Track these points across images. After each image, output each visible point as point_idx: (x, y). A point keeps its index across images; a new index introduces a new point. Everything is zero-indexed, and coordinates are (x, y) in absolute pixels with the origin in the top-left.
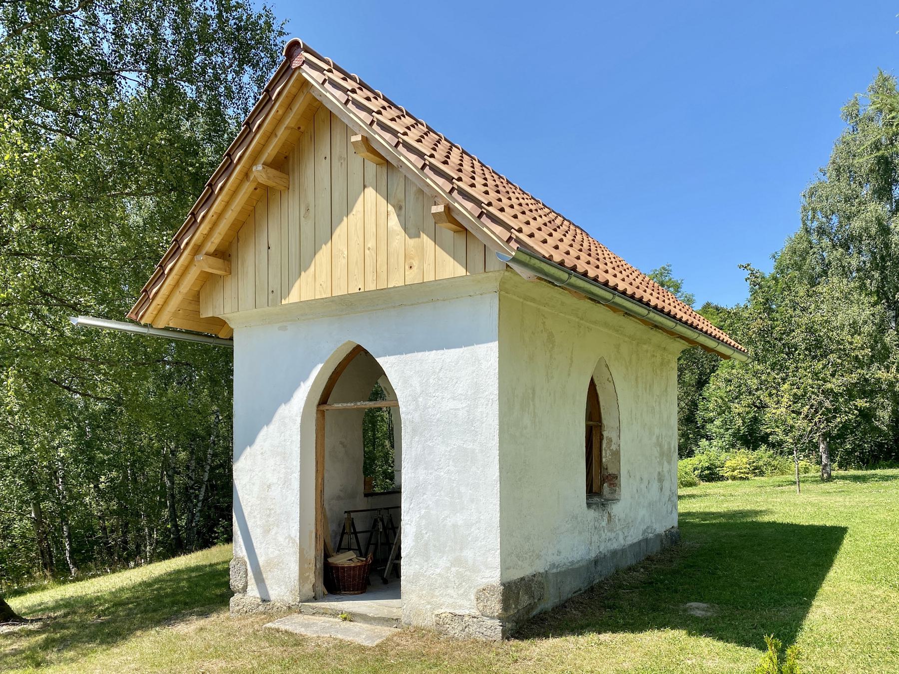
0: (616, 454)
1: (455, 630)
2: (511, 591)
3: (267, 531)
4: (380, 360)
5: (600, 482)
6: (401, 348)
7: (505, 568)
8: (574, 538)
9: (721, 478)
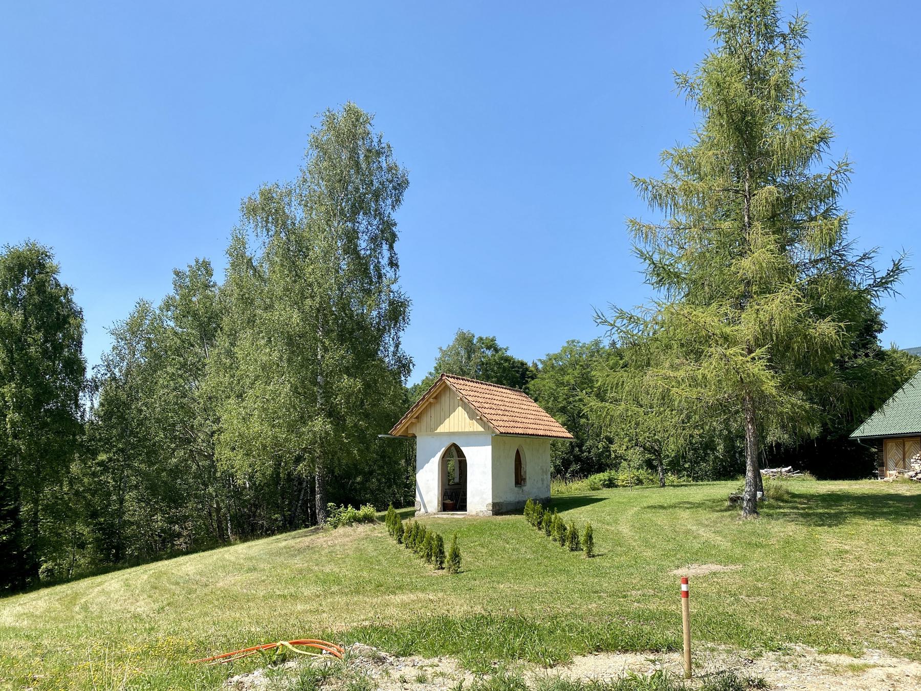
0: (525, 472)
1: (481, 514)
2: (494, 505)
3: (427, 493)
4: (463, 449)
5: (520, 480)
6: (468, 445)
7: (493, 499)
8: (511, 495)
9: (617, 486)
